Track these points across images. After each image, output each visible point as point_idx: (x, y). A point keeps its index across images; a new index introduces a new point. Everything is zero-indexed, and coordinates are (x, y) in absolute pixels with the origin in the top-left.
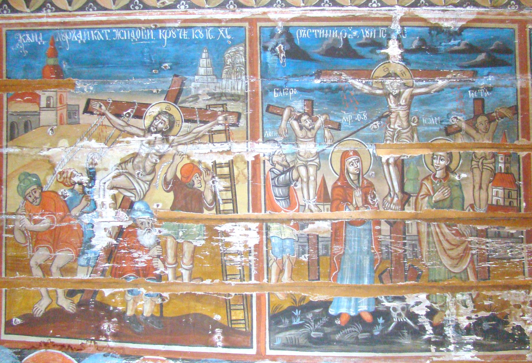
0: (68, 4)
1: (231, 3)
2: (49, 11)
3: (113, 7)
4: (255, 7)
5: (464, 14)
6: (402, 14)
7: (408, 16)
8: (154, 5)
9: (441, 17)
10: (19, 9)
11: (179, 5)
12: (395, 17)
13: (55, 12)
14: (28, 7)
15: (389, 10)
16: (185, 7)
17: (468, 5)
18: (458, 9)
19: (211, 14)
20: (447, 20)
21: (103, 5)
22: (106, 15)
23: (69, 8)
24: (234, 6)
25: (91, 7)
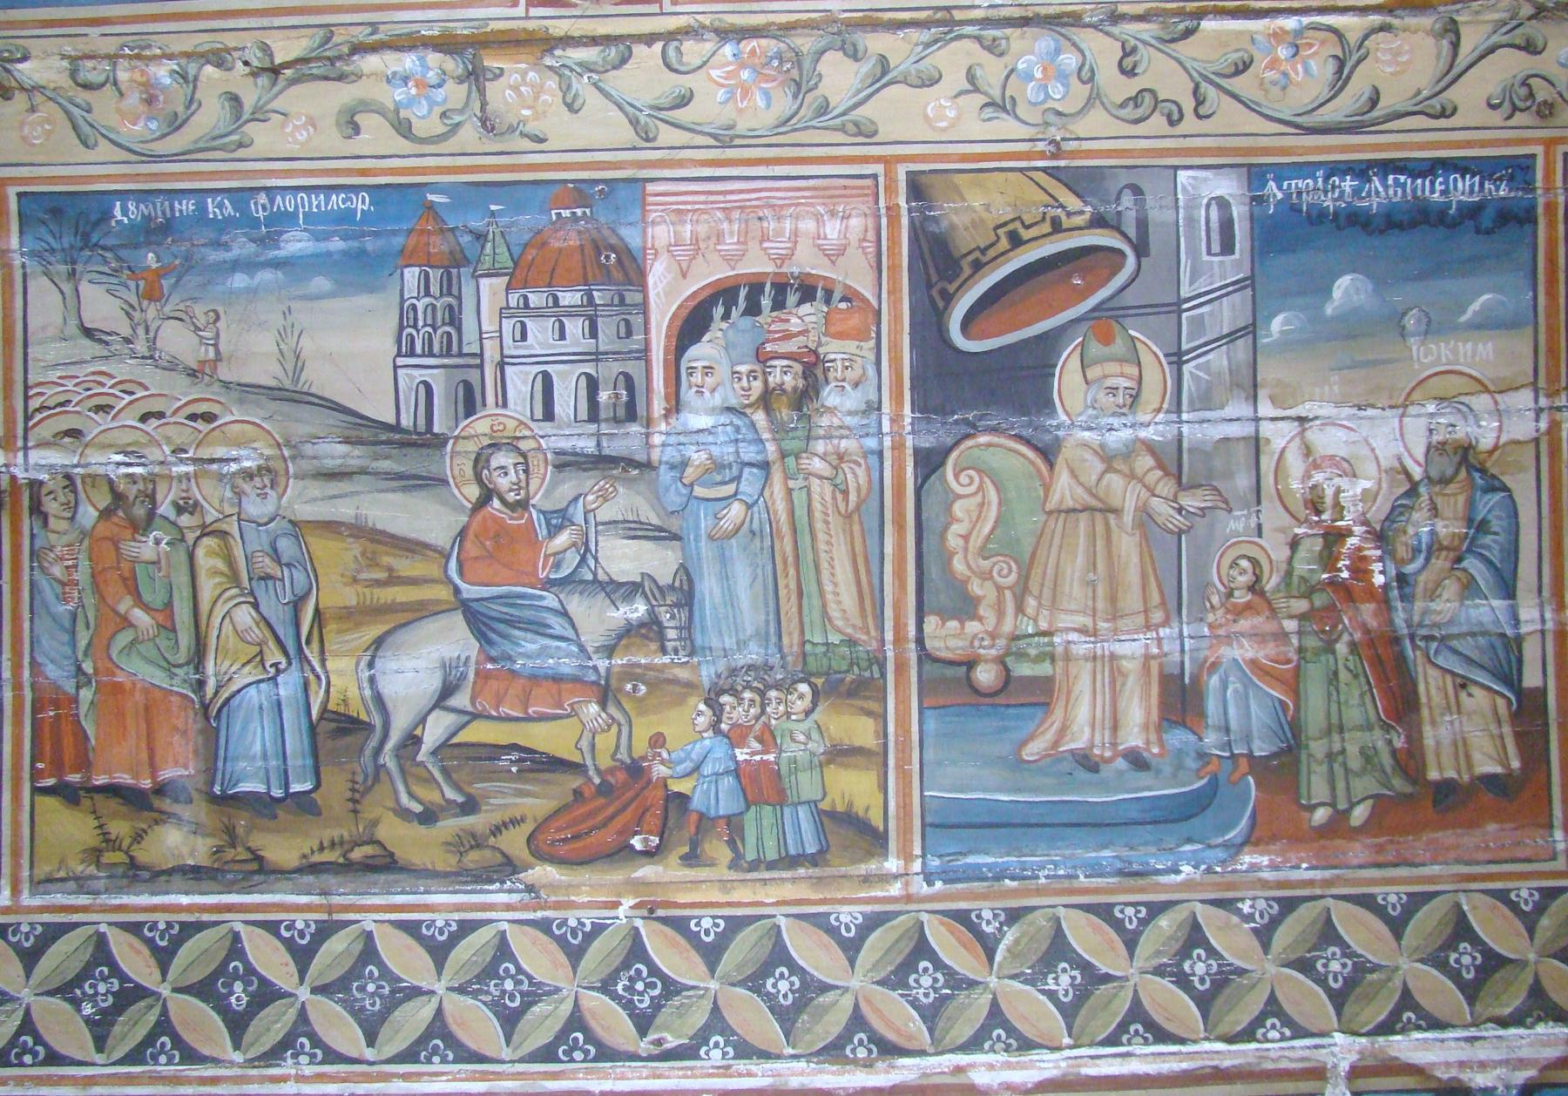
0: (364, 1043)
1: (861, 1042)
2: (304, 1059)
3: (506, 1053)
4: (931, 1050)
5: (1531, 1045)
6: (1354, 1057)
7: (1370, 1062)
8: (632, 1049)
9: (1464, 1058)
10: (206, 1051)
11: (704, 1049)
12: (1335, 1066)
13: (322, 1063)
14: (237, 1046)
15: (1316, 1047)
16: (724, 1054)
17: (1539, 1019)
18: (1512, 1031)
19: (802, 1074)
20: (1483, 1065)
21: (473, 1046)
22: (484, 1076)
23: (369, 1054)
24: (870, 1051)
25: (436, 1049)
